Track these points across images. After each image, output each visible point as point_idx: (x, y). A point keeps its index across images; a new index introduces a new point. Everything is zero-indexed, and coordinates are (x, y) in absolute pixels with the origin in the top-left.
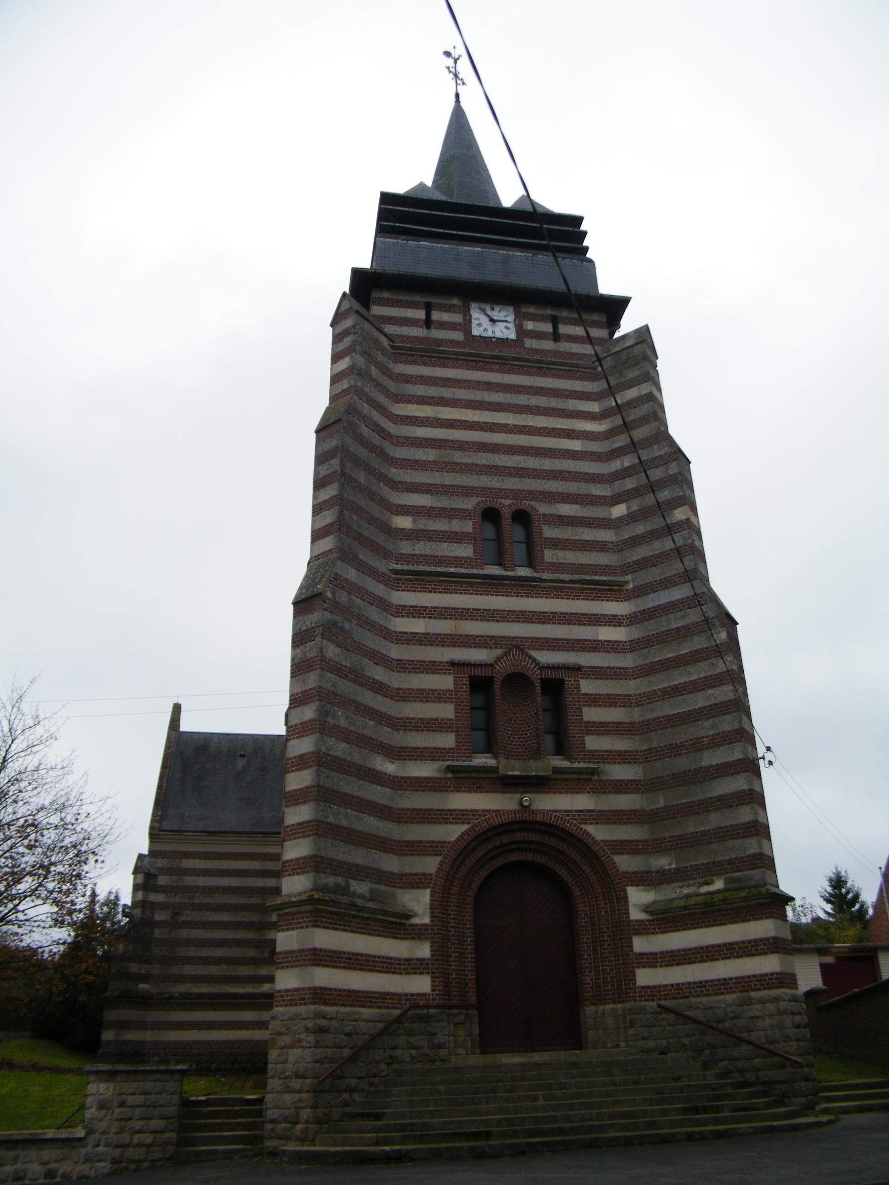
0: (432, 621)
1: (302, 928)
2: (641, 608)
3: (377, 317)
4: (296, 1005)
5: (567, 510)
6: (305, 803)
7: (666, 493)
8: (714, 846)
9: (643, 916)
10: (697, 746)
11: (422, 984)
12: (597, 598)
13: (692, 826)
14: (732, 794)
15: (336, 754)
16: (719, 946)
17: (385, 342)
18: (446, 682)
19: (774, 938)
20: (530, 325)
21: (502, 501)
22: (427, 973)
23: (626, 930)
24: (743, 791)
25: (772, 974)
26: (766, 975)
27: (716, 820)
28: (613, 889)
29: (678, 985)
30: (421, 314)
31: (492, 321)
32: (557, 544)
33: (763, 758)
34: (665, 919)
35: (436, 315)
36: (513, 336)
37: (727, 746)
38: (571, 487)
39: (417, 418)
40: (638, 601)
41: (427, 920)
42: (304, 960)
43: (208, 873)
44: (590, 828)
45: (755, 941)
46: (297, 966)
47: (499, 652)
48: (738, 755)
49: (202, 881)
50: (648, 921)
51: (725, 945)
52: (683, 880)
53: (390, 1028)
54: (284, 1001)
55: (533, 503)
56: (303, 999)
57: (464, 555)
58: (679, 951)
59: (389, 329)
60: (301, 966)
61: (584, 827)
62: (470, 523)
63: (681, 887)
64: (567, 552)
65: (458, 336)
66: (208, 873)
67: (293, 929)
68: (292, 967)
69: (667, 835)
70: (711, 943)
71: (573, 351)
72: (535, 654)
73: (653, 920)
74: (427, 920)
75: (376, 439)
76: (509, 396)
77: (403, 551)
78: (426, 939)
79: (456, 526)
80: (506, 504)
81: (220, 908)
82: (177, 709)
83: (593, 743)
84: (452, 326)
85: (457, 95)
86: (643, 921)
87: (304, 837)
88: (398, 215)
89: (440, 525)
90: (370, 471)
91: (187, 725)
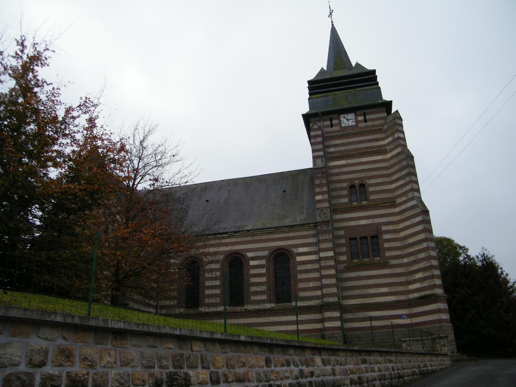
12: (359, 158)
30: (329, 123)
31: (348, 120)
35: (368, 117)
83: (388, 254)
85: (332, 22)
88: (316, 87)
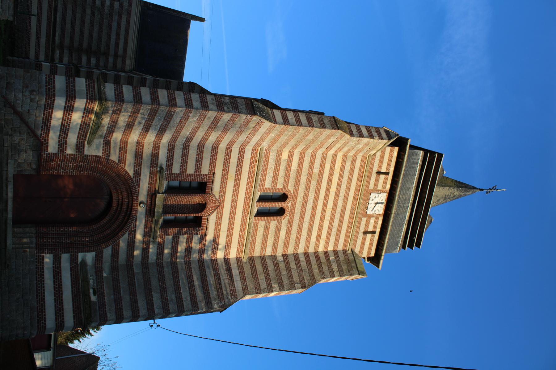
0: (236, 166)
1: (87, 93)
2: (232, 266)
3: (385, 149)
4: (46, 86)
5: (283, 233)
6: (151, 99)
7: (286, 282)
8: (112, 297)
9: (80, 259)
10: (163, 291)
11: (52, 146)
13: (124, 285)
14: (138, 307)
15: (174, 116)
16: (62, 297)
17: (373, 152)
18: (205, 170)
19: (64, 325)
20: (372, 220)
21: (290, 203)
22: (58, 151)
23: (74, 249)
24: (139, 313)
25: (45, 324)
26: (45, 321)
27: (126, 299)
28: (95, 246)
29: (43, 275)
32: (267, 228)
33: (154, 323)
34: (78, 270)
36: (368, 212)
37: (161, 306)
38: (293, 236)
39: (335, 165)
40: (236, 265)
41: (86, 152)
42: (70, 92)
43: (119, 28)
44: (126, 236)
45: (63, 316)
46: (67, 88)
47: (217, 197)
48: (157, 311)
49: (115, 24)
50: (77, 261)
51: (62, 300)
52: (97, 281)
53: (32, 132)
54: (49, 80)
55: (288, 217)
56: (49, 90)
57: (266, 183)
58: (61, 276)
59: (379, 154)
60: (67, 91)
61: (127, 233)
62: (281, 187)
63: (93, 279)
64: (262, 232)
65: (371, 187)
66: (119, 28)
67: (86, 88)
68: (67, 86)
69: (120, 273)
70: (64, 293)
71: (358, 240)
72: (215, 214)
73: (77, 264)
74: (86, 152)
75: (326, 146)
76: (340, 209)
77: (271, 154)
78: (76, 152)
79: (281, 180)
80: (287, 205)
81: (100, 32)
82: (202, 20)
84: (376, 184)
86: (77, 259)
87: (134, 97)
89: (282, 173)
90: (312, 141)
91: (193, 23)
